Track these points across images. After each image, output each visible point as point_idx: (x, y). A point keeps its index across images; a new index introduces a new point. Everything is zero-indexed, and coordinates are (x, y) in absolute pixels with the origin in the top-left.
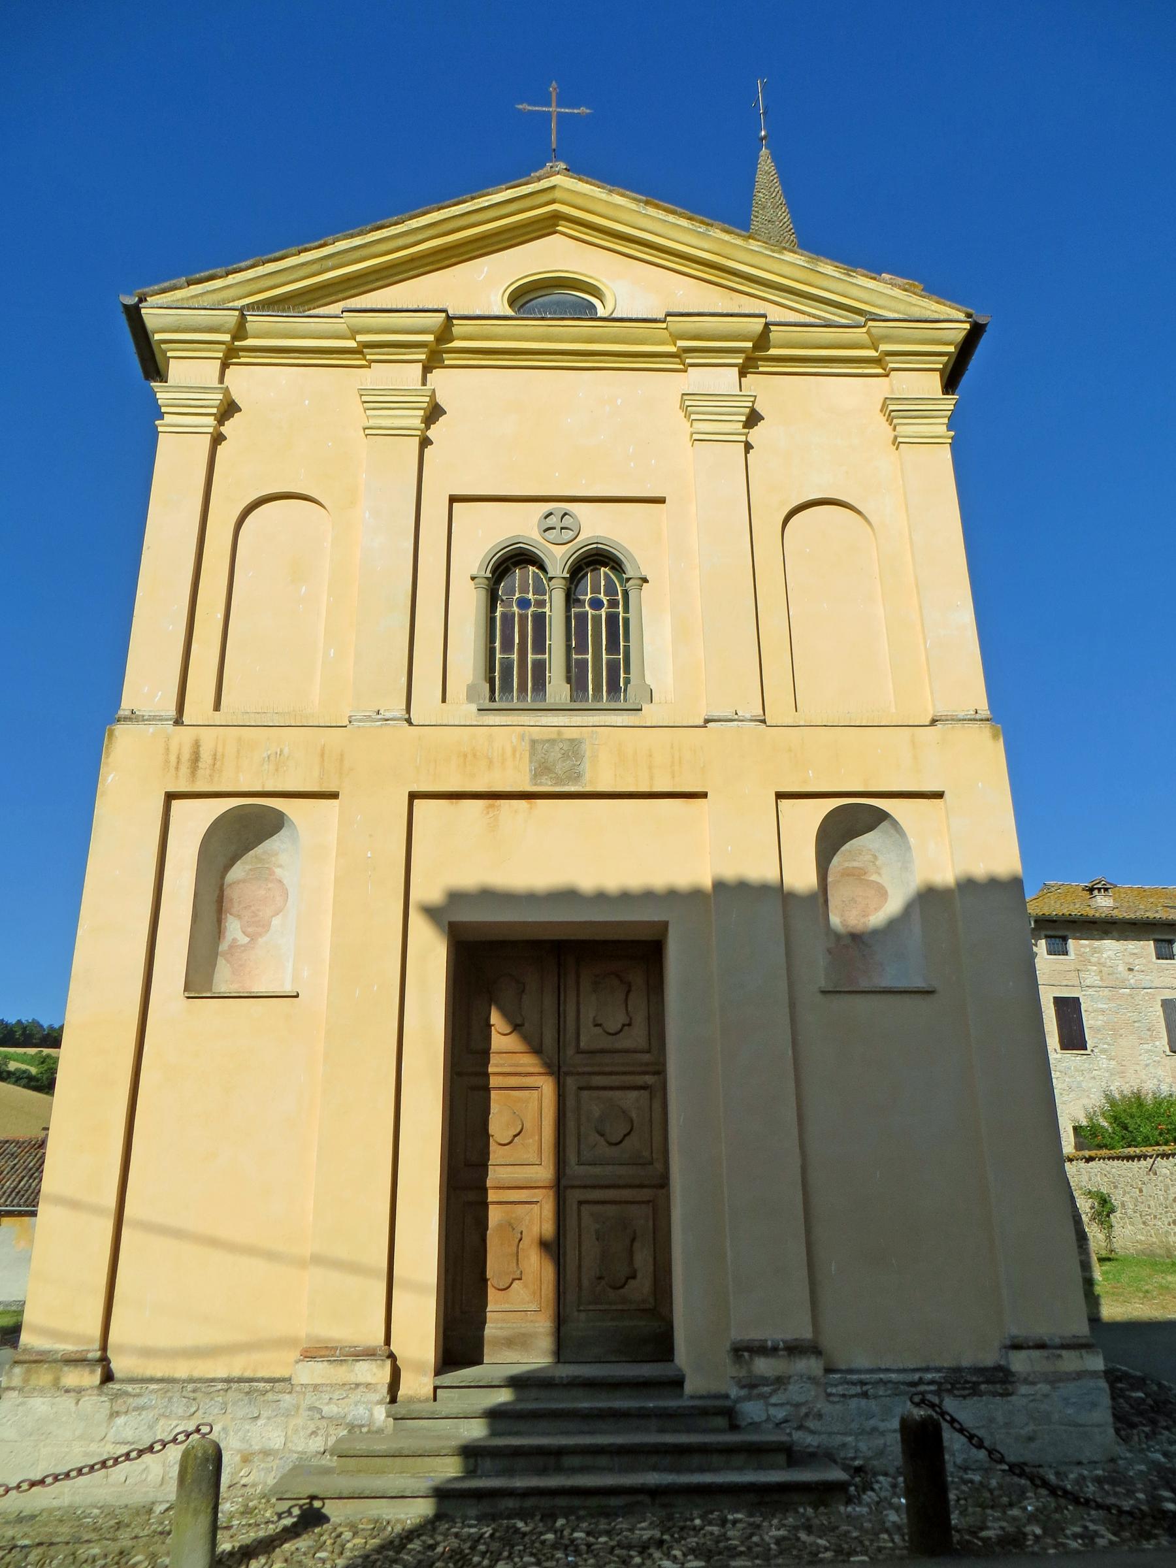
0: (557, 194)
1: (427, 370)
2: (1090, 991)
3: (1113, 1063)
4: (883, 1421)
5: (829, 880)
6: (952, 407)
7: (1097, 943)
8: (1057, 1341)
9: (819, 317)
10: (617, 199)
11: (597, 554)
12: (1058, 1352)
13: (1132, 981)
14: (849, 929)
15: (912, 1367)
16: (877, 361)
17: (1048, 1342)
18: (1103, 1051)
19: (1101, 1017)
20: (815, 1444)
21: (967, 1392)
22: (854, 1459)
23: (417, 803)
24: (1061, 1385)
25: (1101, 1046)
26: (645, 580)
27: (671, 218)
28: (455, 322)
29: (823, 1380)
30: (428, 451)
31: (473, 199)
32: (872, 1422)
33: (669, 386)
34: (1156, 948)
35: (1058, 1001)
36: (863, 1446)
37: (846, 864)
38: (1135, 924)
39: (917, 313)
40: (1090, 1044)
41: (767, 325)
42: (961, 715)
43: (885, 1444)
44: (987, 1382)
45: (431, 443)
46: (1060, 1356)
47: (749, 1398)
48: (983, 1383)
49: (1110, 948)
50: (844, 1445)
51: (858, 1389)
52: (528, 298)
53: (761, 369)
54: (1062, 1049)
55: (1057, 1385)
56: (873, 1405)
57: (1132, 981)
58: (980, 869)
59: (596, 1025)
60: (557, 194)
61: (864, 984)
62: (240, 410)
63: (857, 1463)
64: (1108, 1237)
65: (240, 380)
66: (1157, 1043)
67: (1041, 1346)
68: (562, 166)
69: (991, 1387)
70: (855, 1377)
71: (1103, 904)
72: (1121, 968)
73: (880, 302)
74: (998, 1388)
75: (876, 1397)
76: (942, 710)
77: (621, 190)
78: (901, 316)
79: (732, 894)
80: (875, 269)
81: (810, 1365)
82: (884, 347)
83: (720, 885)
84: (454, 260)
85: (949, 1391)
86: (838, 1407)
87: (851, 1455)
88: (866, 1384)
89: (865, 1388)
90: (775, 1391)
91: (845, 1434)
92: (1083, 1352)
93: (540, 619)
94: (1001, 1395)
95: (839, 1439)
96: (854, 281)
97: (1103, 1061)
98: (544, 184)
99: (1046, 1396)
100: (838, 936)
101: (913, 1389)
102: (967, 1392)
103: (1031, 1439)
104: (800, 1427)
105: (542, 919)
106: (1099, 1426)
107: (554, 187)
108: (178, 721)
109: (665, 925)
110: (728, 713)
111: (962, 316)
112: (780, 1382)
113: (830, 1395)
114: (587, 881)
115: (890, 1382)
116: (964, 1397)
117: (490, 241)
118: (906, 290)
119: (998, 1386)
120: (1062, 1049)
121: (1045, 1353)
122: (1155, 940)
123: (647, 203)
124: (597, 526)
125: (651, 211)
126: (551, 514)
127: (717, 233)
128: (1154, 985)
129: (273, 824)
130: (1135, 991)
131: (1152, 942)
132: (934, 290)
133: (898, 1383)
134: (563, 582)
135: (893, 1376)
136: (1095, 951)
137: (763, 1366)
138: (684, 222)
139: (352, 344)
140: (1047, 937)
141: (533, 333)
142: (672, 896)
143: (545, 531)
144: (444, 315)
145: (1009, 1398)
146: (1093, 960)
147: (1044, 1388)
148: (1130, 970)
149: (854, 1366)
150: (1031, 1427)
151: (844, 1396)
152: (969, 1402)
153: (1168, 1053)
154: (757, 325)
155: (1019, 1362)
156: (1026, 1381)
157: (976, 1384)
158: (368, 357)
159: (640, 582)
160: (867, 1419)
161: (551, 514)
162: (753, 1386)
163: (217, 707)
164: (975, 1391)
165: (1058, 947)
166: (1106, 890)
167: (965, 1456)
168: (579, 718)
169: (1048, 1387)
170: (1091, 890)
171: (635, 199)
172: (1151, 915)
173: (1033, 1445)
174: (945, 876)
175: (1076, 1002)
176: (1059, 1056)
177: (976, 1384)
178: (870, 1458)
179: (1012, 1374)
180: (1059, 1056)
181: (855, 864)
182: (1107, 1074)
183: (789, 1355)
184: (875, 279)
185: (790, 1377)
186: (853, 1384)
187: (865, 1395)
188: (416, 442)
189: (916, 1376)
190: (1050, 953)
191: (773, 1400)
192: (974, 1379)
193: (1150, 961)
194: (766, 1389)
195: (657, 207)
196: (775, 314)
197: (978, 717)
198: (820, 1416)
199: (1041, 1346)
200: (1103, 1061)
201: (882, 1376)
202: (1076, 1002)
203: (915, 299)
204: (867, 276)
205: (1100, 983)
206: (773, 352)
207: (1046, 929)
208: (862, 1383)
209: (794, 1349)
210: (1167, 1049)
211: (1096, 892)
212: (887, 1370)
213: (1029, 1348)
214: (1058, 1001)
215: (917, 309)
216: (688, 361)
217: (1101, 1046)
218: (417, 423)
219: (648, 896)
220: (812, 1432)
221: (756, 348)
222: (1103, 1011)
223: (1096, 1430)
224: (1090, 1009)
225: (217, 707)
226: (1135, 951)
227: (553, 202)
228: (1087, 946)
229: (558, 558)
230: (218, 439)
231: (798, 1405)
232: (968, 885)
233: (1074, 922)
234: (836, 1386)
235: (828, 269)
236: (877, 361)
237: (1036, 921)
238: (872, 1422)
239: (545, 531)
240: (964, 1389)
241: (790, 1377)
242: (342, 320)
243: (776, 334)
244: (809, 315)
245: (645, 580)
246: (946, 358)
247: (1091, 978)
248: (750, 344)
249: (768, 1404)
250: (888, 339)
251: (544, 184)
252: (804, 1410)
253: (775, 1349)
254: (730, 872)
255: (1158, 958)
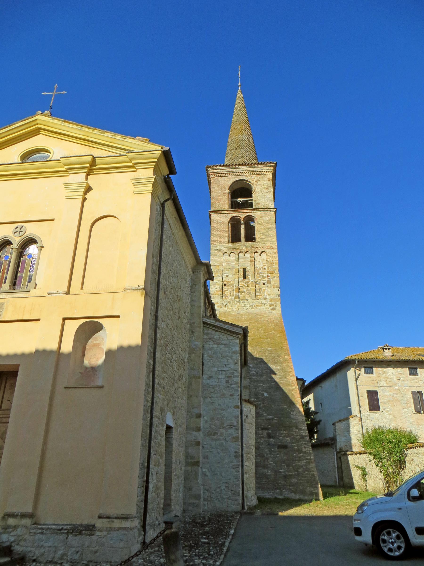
0: (38, 122)
1: (88, 175)
2: (382, 388)
3: (391, 416)
4: (46, 543)
5: (87, 348)
6: (85, 185)
7: (385, 370)
8: (115, 516)
9: (119, 154)
10: (56, 121)
11: (31, 240)
12: (113, 520)
13: (399, 384)
14: (92, 365)
15: (66, 524)
16: (133, 167)
17: (111, 516)
18: (387, 412)
19: (386, 398)
20: (21, 550)
21: (77, 534)
22: (33, 556)
23: (67, 322)
24: (111, 532)
25: (386, 410)
26: (43, 247)
27: (71, 126)
28: (96, 159)
29: (29, 527)
30: (85, 203)
31: (10, 126)
32: (42, 543)
33: (58, 182)
34: (410, 371)
35: (369, 392)
36: (37, 552)
37: (94, 342)
38: (399, 362)
39: (145, 149)
40: (381, 409)
41: (94, 158)
42: (133, 288)
43: (44, 552)
44: (86, 530)
45: (87, 199)
46: (113, 521)
47: (4, 533)
48: (83, 530)
49: (390, 371)
50: (30, 551)
51: (41, 531)
52: (26, 157)
53: (95, 173)
54: (370, 411)
55: (110, 532)
56: (44, 537)
57: (399, 384)
58: (126, 343)
59: (8, 401)
60: (38, 122)
61: (92, 385)
62: (92, 189)
63: (34, 558)
64: (366, 485)
65: (93, 180)
66: (410, 409)
67: (108, 517)
68: (40, 112)
69: (86, 532)
70: (41, 526)
71: (388, 354)
72: (395, 379)
73: (134, 147)
74: (89, 532)
75: (46, 534)
76: (127, 286)
77: (57, 118)
78: (142, 151)
79: (41, 354)
80: (134, 135)
81: (27, 522)
82: (134, 162)
83: (37, 351)
84: (5, 146)
85: (72, 533)
86: (32, 537)
87: (32, 555)
88: (43, 529)
89: (43, 531)
90: (13, 531)
91: (32, 547)
92: (122, 520)
93: (10, 262)
94: (89, 535)
95: (29, 549)
96: (126, 140)
97: (387, 415)
98: (34, 118)
99: (105, 536)
100: (86, 368)
101: (59, 532)
102: (77, 534)
103: (96, 552)
104: (18, 544)
105: (7, 364)
106: (121, 548)
107: (36, 120)
108: (68, 293)
109: (18, 366)
110: (55, 291)
111: (160, 148)
112: (15, 527)
113: (30, 533)
114: (319, 375)
115: (52, 529)
116: (76, 535)
117: (21, 137)
118: (143, 142)
119: (89, 532)
120: (370, 411)
121: (108, 520)
122: (409, 368)
123: (64, 121)
124: (31, 230)
125: (65, 124)
126: (18, 227)
127: (85, 129)
128: (409, 386)
129: (98, 328)
130: (400, 388)
131: (408, 369)
132: (153, 141)
133: (54, 529)
134: (16, 250)
135: (54, 527)
136: (384, 372)
137: (11, 521)
138: (75, 126)
139: (131, 164)
140: (364, 367)
141: (30, 167)
142: (23, 355)
143: (14, 233)
144: (92, 157)
145: (92, 537)
146: (383, 376)
147: (105, 533)
148: (399, 380)
149: (46, 523)
150: (97, 548)
151: (35, 533)
152: (77, 537)
153: (414, 412)
154: (90, 159)
155: (99, 524)
156: (99, 530)
157: (81, 531)
158: (136, 168)
159: (41, 248)
160: (41, 542)
161: (18, 227)
162: (6, 529)
163: (82, 288)
164: (80, 533)
165: (369, 371)
166: (389, 349)
167: (70, 557)
168: (20, 295)
169: (107, 533)
170: (383, 349)
171: (61, 121)
172: (406, 358)
173: (96, 554)
174: (114, 346)
175: (376, 392)
176: (369, 414)
177: (81, 531)
178: (38, 557)
179: (95, 528)
180: (369, 414)
181: (97, 342)
182: (388, 421)
183: (20, 518)
184: (133, 139)
185: (19, 526)
186: (40, 529)
187: (42, 533)
188: (81, 200)
189: (61, 527)
190: (366, 373)
191: (12, 534)
192: (81, 529)
193: (407, 376)
194: (10, 530)
195: (67, 122)
196: (97, 153)
197: (140, 288)
198: (25, 540)
199: (108, 517)
200: (387, 415)
201: (49, 527)
202: (376, 392)
203: (145, 144)
204: (131, 138)
205: (386, 385)
206: (97, 167)
207: (364, 364)
208: (43, 529)
209: (23, 516)
210: (414, 411)
211: (385, 350)
212: (63, 525)
213: (104, 518)
214: (369, 392)
215: (145, 148)
216: (69, 172)
217: (386, 410)
218: (82, 193)
219: (15, 356)
220: (21, 546)
221: (91, 166)
222: (387, 396)
223: (120, 550)
224: (382, 395)
225: (82, 288)
226: (401, 372)
227: (37, 124)
228: (381, 371)
229: (16, 241)
230: (84, 200)
231: (19, 536)
232: (121, 349)
233: (374, 361)
234: (34, 529)
235: (119, 137)
236: (133, 167)
237: (358, 361)
238: (42, 543)
239: (14, 233)
240: (77, 532)
241: (19, 526)
242: (126, 157)
243: (98, 161)
244: (116, 153)
245: (43, 247)
246: (155, 164)
247: (382, 383)
248: (88, 165)
249: (9, 535)
250: (134, 159)
251: (34, 118)
252: (20, 538)
253: (17, 515)
254: (41, 347)
255: (410, 375)
